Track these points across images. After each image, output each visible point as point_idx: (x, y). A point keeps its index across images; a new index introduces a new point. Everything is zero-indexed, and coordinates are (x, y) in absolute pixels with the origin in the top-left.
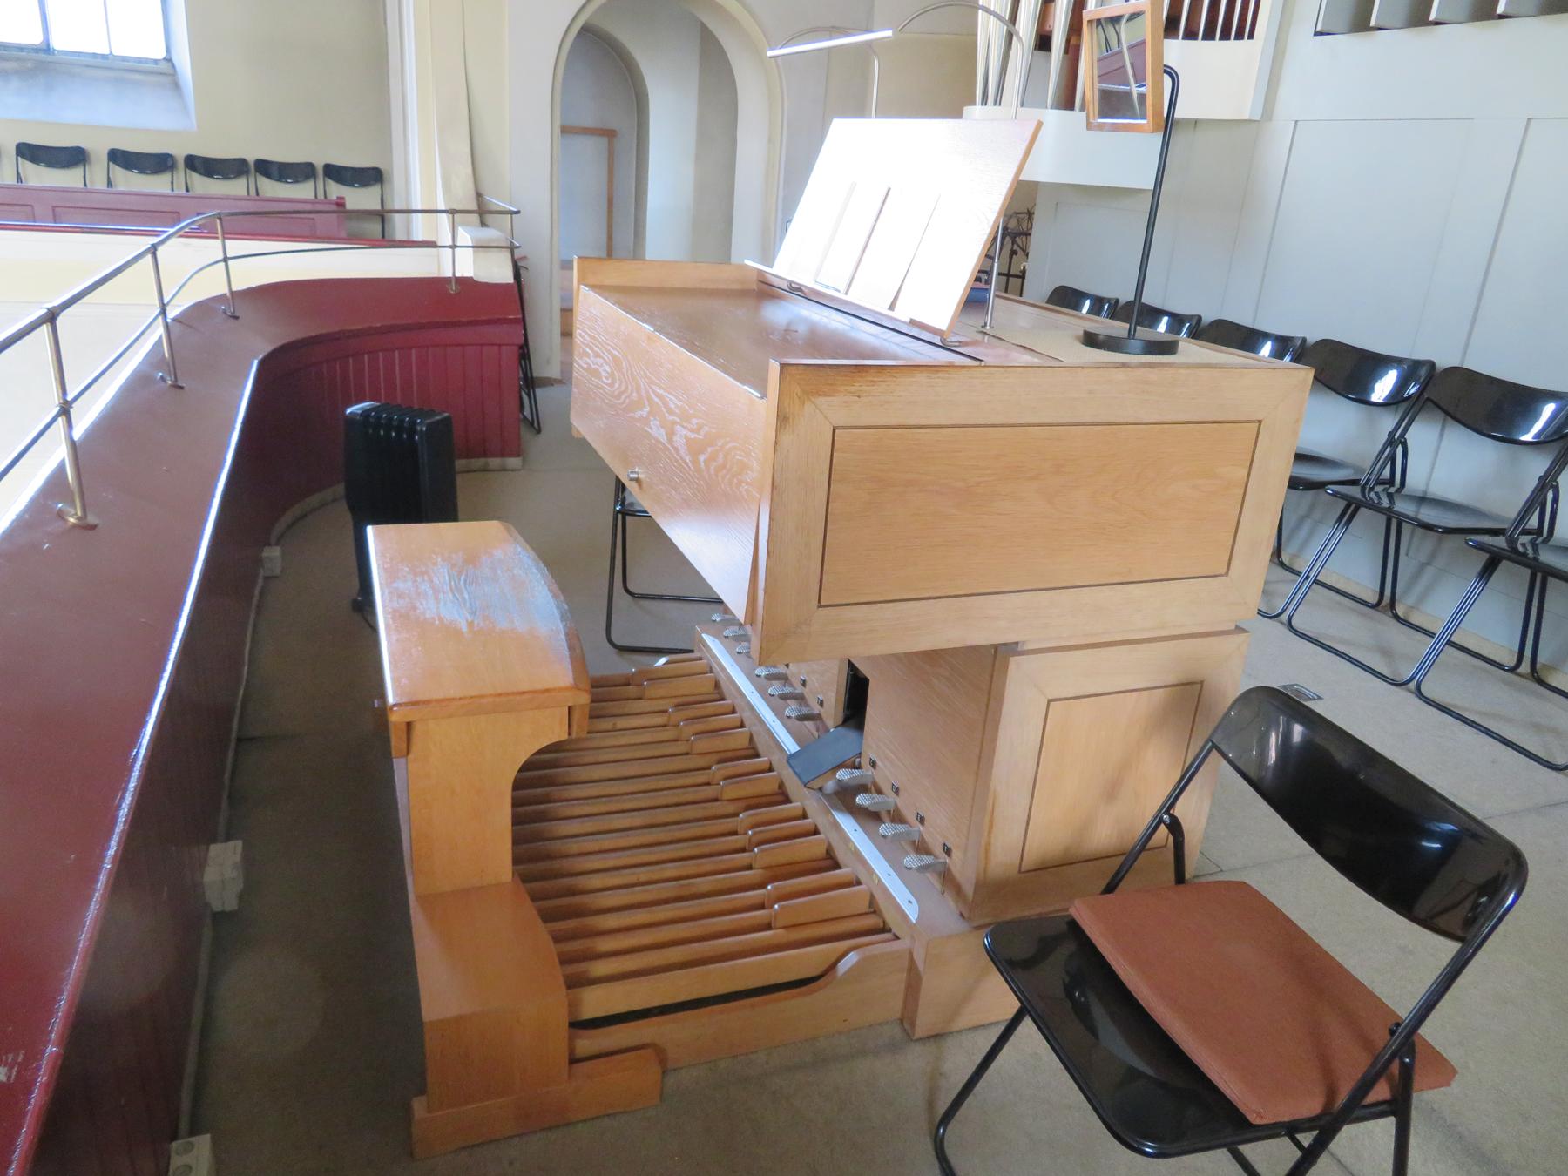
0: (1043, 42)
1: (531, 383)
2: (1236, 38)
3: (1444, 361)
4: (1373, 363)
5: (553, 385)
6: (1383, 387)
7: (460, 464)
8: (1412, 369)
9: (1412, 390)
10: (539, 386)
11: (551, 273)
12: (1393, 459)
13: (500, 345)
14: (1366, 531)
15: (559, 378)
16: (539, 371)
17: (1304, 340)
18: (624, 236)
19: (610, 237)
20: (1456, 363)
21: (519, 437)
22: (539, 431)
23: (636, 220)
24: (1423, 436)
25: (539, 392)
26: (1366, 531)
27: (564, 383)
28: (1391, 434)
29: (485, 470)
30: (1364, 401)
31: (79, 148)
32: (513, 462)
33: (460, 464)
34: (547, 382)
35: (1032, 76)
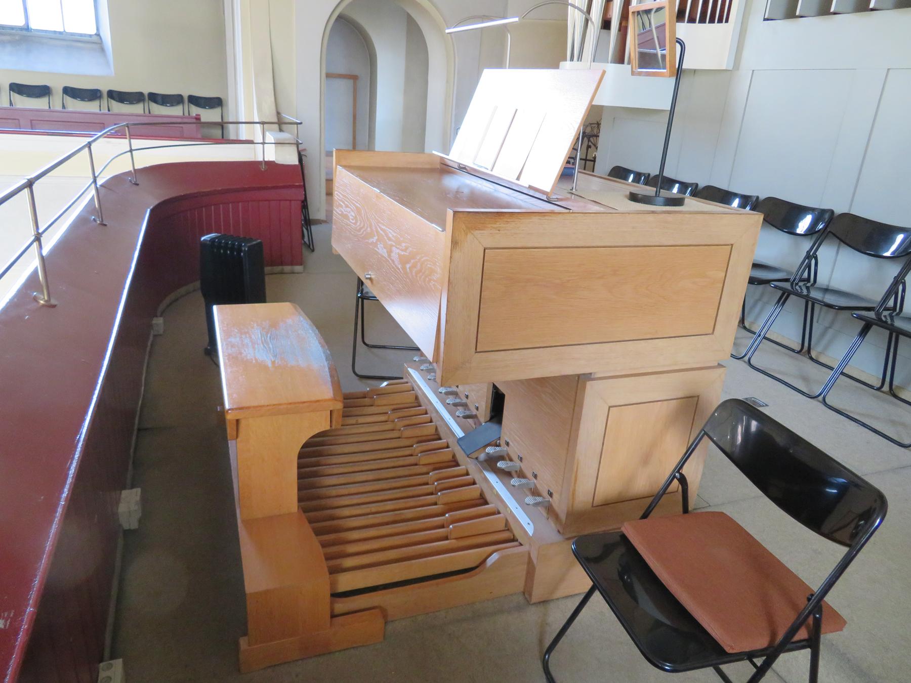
0: (606, 24)
1: (308, 222)
2: (718, 22)
3: (839, 210)
4: (798, 211)
5: (321, 224)
6: (804, 225)
7: (267, 269)
8: (821, 215)
9: (821, 226)
10: (313, 224)
11: (320, 158)
12: (809, 267)
13: (290, 201)
14: (794, 309)
15: (325, 219)
16: (313, 215)
17: (758, 197)
18: (363, 137)
19: (354, 138)
20: (846, 211)
21: (301, 254)
22: (313, 251)
23: (370, 128)
24: (827, 253)
25: (313, 228)
26: (794, 309)
27: (328, 223)
28: (808, 252)
29: (282, 273)
30: (793, 233)
31: (46, 86)
32: (298, 268)
33: (267, 269)
34: (318, 222)
35: (600, 44)
